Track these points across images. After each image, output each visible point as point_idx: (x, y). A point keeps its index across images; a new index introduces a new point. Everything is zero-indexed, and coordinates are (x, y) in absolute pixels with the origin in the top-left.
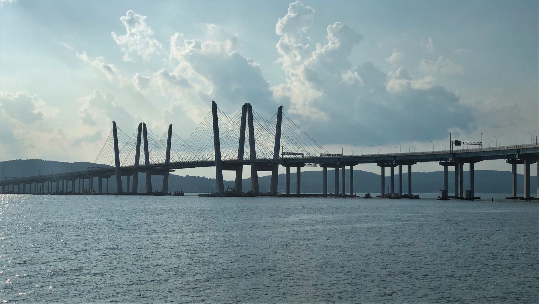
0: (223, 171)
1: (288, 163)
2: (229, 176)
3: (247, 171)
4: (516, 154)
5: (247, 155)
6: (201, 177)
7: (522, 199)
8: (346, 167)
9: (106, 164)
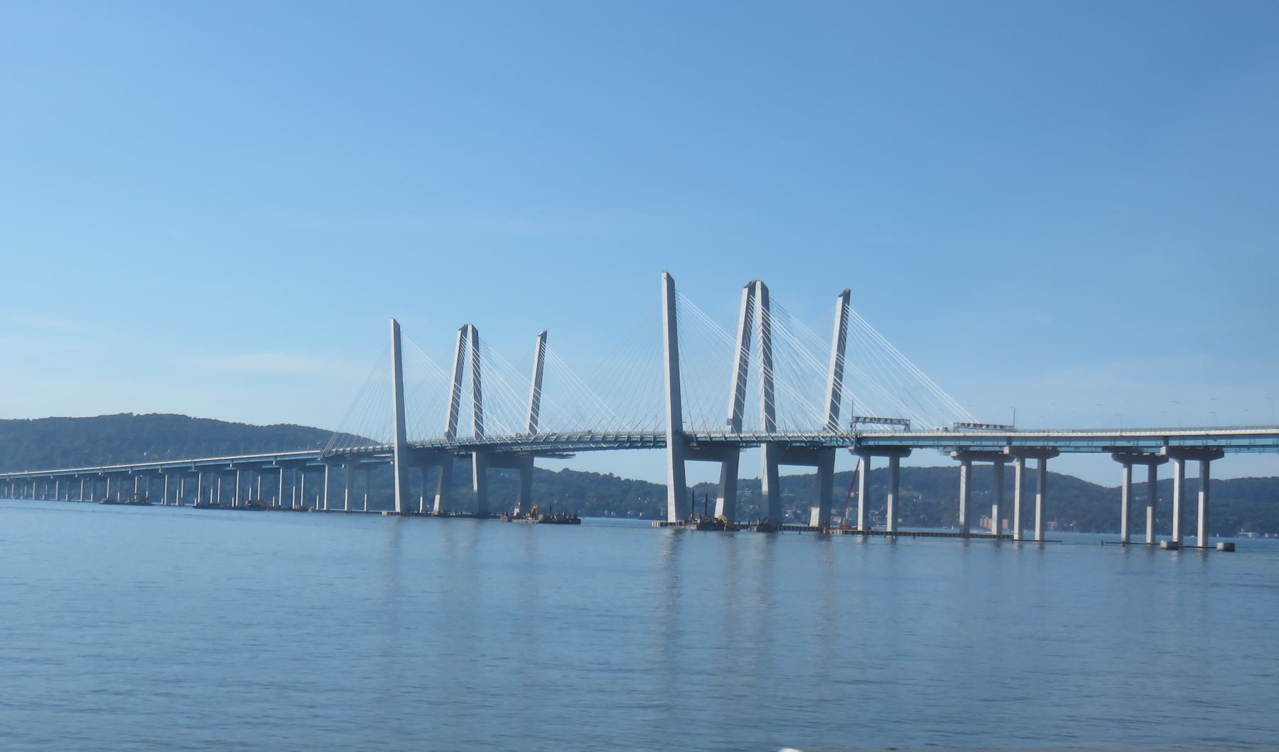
0: (779, 466)
1: (864, 447)
2: (704, 472)
3: (753, 465)
4: (1161, 447)
5: (755, 423)
6: (602, 474)
7: (453, 516)
8: (1027, 461)
9: (367, 437)
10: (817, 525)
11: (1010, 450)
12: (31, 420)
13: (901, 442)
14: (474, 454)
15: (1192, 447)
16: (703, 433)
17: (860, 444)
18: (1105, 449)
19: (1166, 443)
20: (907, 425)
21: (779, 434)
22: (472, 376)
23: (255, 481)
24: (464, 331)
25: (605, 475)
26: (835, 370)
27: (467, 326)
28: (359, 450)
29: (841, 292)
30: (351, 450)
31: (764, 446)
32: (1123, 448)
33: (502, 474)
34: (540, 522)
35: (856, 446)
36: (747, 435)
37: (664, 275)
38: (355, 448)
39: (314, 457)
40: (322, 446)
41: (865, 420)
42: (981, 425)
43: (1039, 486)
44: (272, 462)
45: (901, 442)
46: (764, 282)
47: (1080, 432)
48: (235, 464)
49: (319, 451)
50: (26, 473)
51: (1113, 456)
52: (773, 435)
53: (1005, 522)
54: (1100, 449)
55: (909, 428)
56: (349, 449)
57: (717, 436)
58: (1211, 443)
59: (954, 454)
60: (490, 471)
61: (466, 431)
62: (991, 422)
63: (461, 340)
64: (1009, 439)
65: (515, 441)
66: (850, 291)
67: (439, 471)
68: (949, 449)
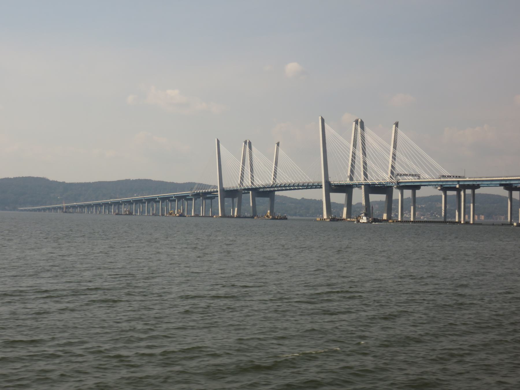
2: (339, 198)
4: (457, 184)
10: (386, 219)
11: (459, 186)
12: (91, 182)
13: (506, 182)
14: (251, 192)
15: (468, 185)
16: (338, 181)
17: (399, 184)
18: (501, 185)
19: (458, 184)
20: (419, 177)
21: (369, 182)
22: (249, 161)
23: (140, 206)
24: (246, 142)
25: (318, 200)
26: (352, 155)
27: (247, 141)
28: (205, 191)
29: (355, 120)
30: (202, 191)
31: (363, 186)
32: (507, 184)
33: (277, 200)
34: (271, 219)
35: (397, 186)
36: (342, 182)
37: (320, 117)
38: (212, 190)
39: (188, 194)
40: (191, 190)
41: (401, 175)
42: (451, 176)
43: (472, 201)
44: (173, 197)
45: (443, 183)
46: (322, 116)
47: (480, 178)
48: (145, 199)
49: (190, 192)
50: (75, 204)
51: (504, 188)
52: (352, 182)
53: (467, 216)
54: (498, 185)
55: (420, 178)
56: (201, 191)
57: (343, 183)
58: (475, 183)
59: (439, 188)
60: (257, 199)
61: (247, 183)
62: (455, 175)
63: (244, 146)
64: (459, 181)
65: (264, 187)
66: (398, 122)
67: (236, 200)
68: (437, 186)
